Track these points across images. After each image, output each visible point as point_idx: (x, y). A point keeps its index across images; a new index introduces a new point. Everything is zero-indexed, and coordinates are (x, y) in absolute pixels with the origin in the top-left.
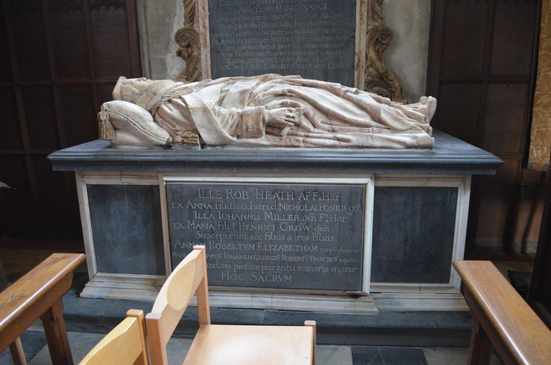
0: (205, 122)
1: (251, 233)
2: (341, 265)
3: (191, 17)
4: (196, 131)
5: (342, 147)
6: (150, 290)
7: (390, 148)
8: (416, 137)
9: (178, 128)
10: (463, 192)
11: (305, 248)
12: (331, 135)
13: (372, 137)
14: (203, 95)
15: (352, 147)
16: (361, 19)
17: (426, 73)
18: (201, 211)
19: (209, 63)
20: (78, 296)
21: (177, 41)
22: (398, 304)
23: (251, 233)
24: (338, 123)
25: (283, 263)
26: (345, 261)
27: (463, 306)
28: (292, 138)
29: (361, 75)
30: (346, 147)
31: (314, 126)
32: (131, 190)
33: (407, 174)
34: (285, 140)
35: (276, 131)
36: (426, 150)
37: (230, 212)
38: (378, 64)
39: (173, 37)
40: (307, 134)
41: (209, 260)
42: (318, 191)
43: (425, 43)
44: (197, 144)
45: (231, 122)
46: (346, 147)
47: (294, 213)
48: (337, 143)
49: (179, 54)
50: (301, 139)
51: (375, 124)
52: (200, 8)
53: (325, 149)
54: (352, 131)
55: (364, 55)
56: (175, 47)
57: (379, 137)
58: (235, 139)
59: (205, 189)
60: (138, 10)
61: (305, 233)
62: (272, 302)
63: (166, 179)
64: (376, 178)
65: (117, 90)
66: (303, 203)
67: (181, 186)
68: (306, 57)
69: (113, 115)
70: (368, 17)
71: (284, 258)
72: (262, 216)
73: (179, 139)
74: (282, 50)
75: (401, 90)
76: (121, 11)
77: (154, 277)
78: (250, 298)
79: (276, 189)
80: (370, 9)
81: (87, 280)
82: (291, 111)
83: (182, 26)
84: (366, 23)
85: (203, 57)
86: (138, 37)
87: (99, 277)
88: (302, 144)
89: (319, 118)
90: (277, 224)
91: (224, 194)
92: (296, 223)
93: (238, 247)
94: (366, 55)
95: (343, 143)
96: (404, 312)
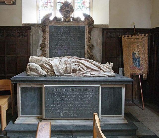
1: (69, 101)
3: (44, 40)
4: (54, 72)
6: (37, 120)
8: (111, 74)
9: (49, 71)
12: (89, 73)
13: (100, 74)
14: (54, 61)
15: (95, 76)
17: (101, 55)
20: (14, 123)
21: (40, 46)
22: (109, 122)
23: (69, 101)
24: (90, 70)
25: (77, 110)
26: (94, 109)
28: (79, 74)
29: (86, 56)
32: (34, 89)
33: (110, 83)
34: (78, 74)
35: (75, 72)
36: (113, 77)
37: (63, 95)
39: (39, 45)
40: (83, 73)
42: (87, 89)
43: (101, 48)
45: (63, 69)
47: (80, 95)
49: (41, 49)
51: (99, 70)
52: (47, 38)
53: (88, 77)
56: (40, 48)
57: (101, 74)
61: (83, 101)
62: (74, 122)
63: (45, 85)
64: (101, 85)
65: (30, 60)
66: (83, 92)
67: (49, 88)
68: (73, 51)
69: (30, 67)
71: (78, 109)
72: (72, 96)
73: (49, 74)
74: (67, 49)
76: (26, 38)
77: (38, 116)
78: (67, 122)
79: (76, 88)
82: (79, 67)
83: (42, 42)
85: (47, 50)
87: (21, 116)
88: (82, 76)
89: (85, 68)
90: (76, 98)
91: (61, 90)
92: (81, 98)
95: (93, 75)
96: (111, 124)
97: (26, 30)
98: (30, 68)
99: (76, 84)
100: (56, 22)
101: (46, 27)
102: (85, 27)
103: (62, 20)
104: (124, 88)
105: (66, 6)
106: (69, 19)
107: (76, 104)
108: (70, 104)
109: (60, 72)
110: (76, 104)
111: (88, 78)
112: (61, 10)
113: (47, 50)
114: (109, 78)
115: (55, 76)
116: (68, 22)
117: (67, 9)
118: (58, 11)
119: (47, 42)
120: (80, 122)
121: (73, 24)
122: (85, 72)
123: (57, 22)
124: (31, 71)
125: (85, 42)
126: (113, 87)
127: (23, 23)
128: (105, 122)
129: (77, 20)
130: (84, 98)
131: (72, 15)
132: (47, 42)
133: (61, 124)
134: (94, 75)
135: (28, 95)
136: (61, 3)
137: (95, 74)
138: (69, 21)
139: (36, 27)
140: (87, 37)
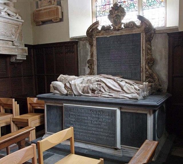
0: (75, 88)
2: (110, 137)
3: (92, 56)
5: (111, 98)
7: (124, 99)
8: (132, 96)
10: (149, 115)
11: (99, 130)
13: (119, 95)
16: (143, 55)
18: (72, 115)
19: (96, 70)
21: (88, 63)
23: (85, 123)
24: (112, 90)
25: (93, 134)
26: (111, 135)
27: (35, 130)
30: (112, 98)
31: (105, 91)
34: (95, 95)
37: (79, 116)
38: (149, 71)
41: (74, 131)
42: (102, 111)
43: (167, 63)
44: (73, 95)
45: (81, 89)
46: (112, 98)
48: (109, 96)
50: (100, 94)
51: (122, 91)
54: (114, 93)
55: (144, 67)
57: (122, 95)
58: (83, 94)
59: (74, 108)
60: (78, 54)
64: (120, 108)
65: (58, 79)
66: (98, 115)
70: (146, 54)
72: (88, 118)
73: (68, 93)
75: (159, 80)
79: (91, 110)
80: (146, 52)
81: (44, 134)
84: (145, 56)
86: (78, 62)
88: (100, 96)
89: (106, 88)
90: (91, 120)
93: (81, 127)
94: (145, 68)
97: (73, 46)
98: (53, 87)
99: (76, 103)
100: (105, 32)
101: (93, 40)
102: (140, 34)
103: (112, 28)
104: (150, 114)
105: (116, 10)
106: (119, 26)
107: (92, 127)
108: (85, 126)
109: (77, 91)
110: (92, 127)
111: (106, 99)
112: (110, 17)
113: (95, 68)
114: (130, 101)
115: (75, 95)
116: (118, 30)
117: (117, 12)
118: (107, 16)
119: (95, 58)
120: (96, 148)
121: (124, 33)
122: (105, 92)
123: (106, 32)
124: (56, 90)
125: (142, 55)
126: (135, 112)
127: (71, 36)
128: (126, 154)
129: (131, 26)
130: (100, 121)
131: (123, 21)
132: (95, 58)
133: (78, 146)
134: (112, 97)
135: (52, 113)
136: (123, 3)
137: (114, 94)
138: (120, 29)
139: (83, 40)
140: (144, 48)
